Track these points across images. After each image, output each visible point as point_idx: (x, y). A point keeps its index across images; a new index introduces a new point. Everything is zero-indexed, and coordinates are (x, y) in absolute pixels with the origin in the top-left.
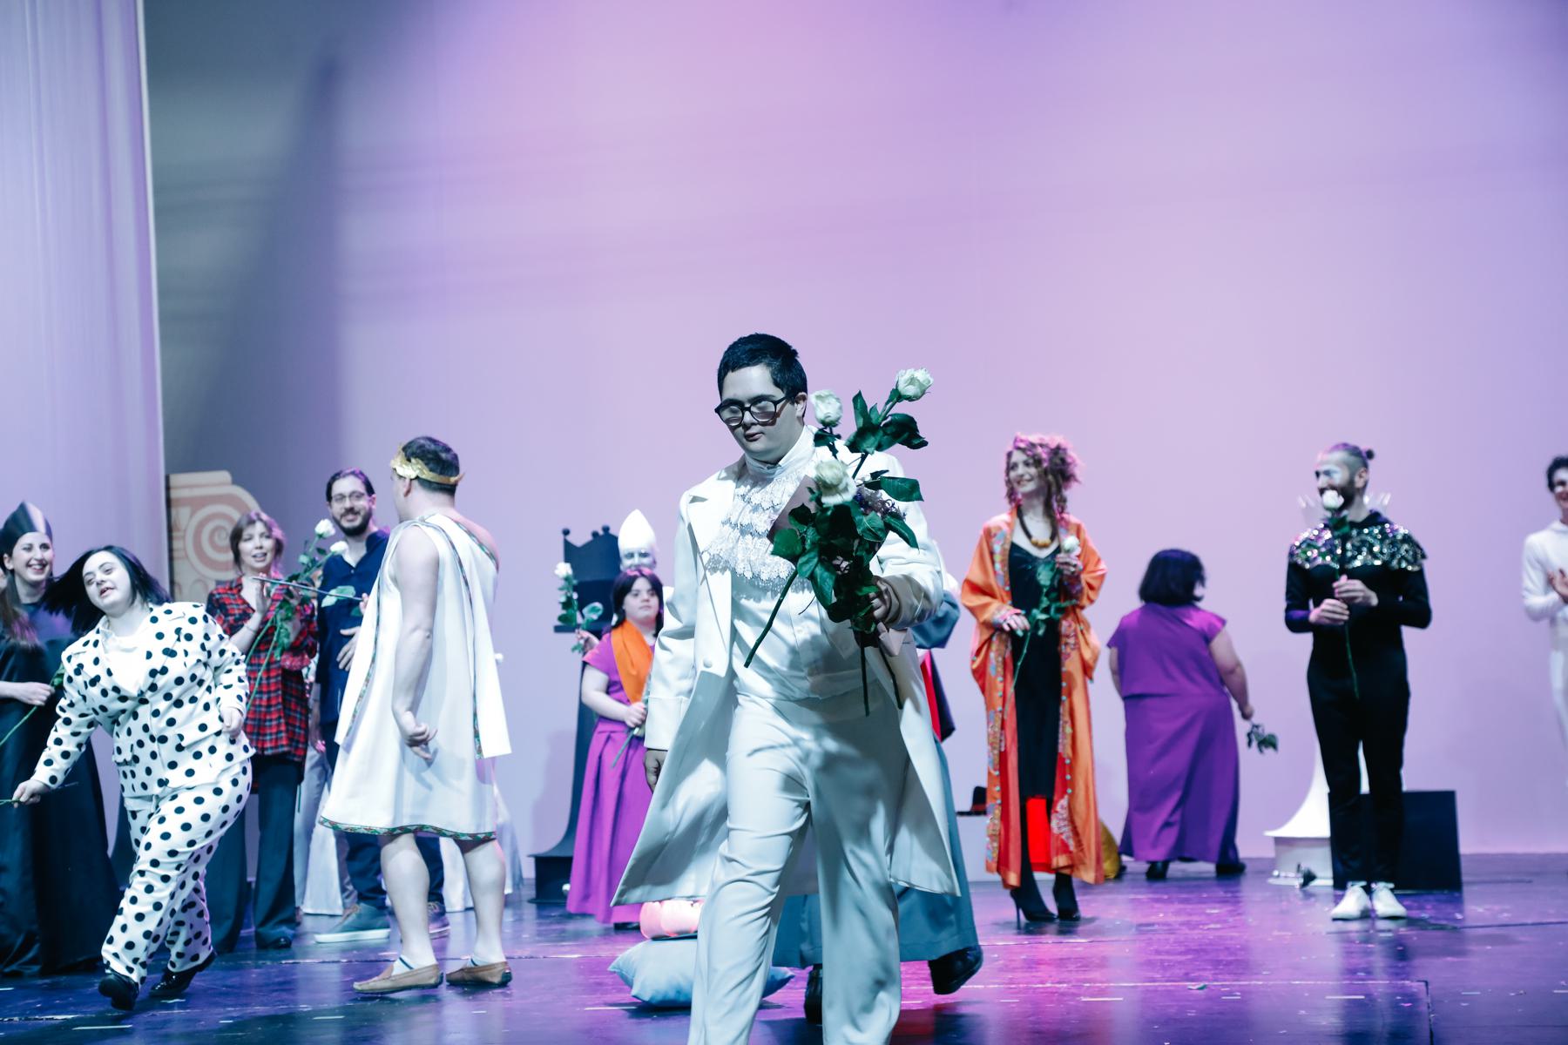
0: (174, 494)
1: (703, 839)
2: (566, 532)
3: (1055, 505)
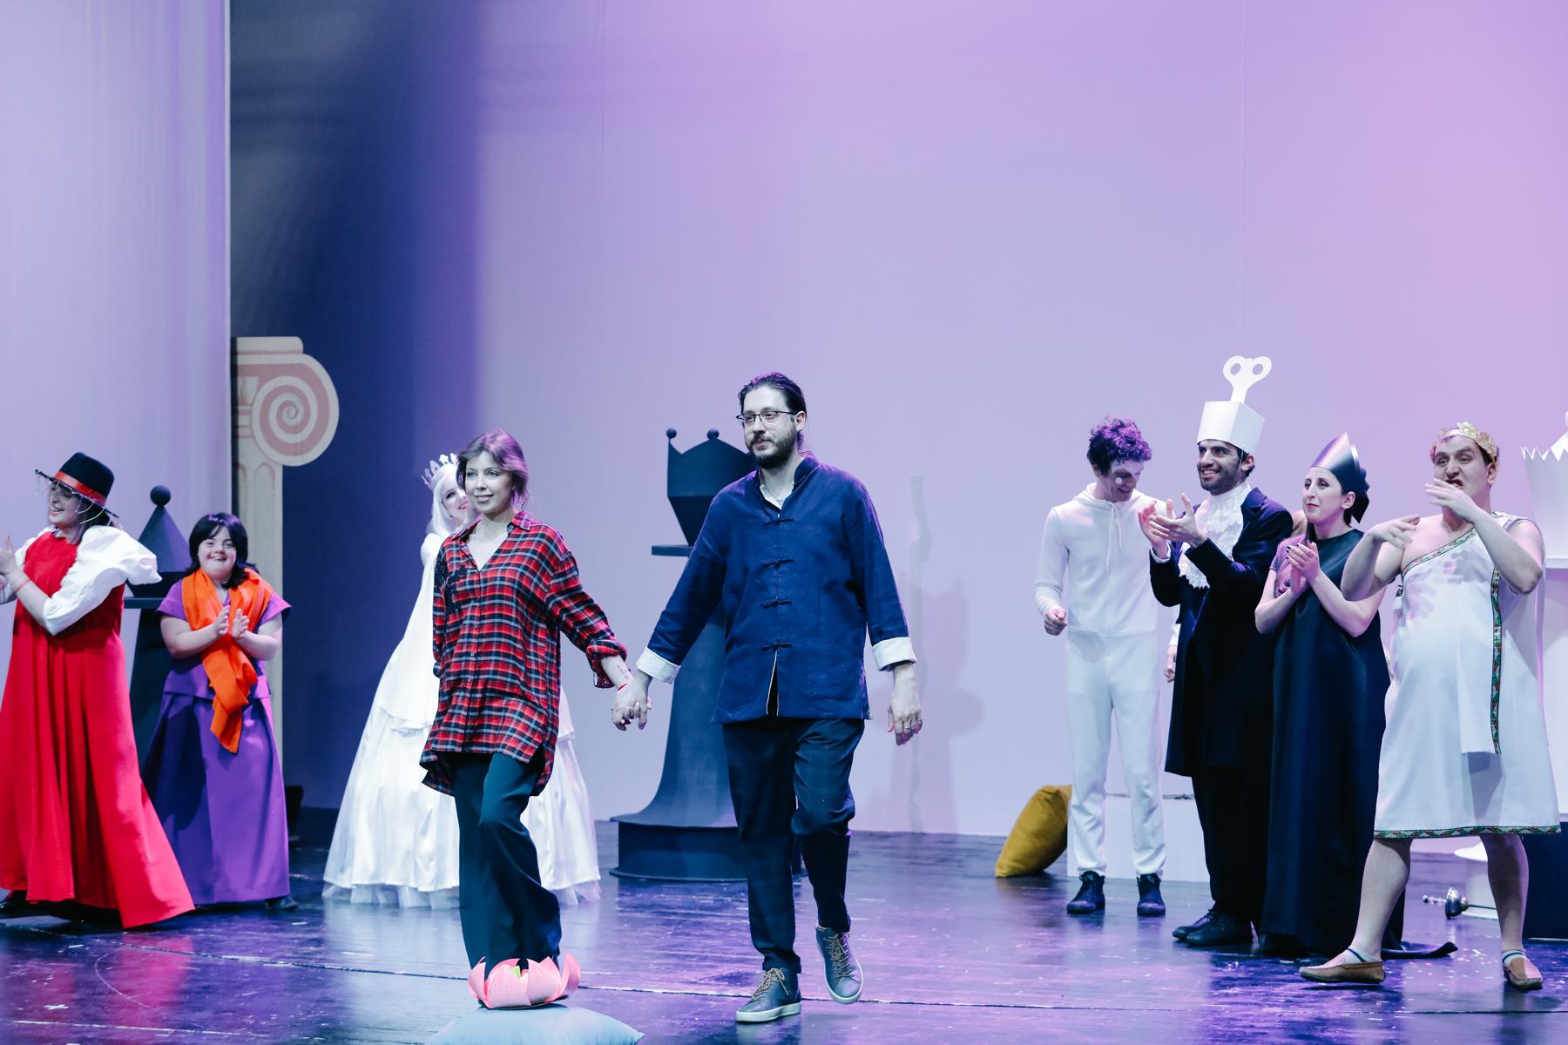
0: (241, 360)
2: (672, 434)
3: (1154, 989)
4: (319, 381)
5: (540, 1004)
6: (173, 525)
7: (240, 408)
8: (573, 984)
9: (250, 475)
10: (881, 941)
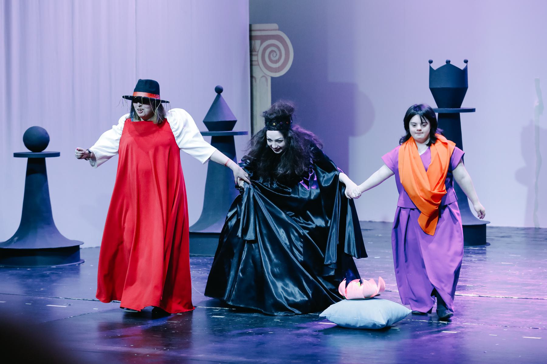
1: (268, 207)
2: (431, 62)
4: (284, 39)
5: (368, 298)
6: (224, 101)
7: (254, 53)
8: (382, 289)
9: (258, 81)
10: (517, 273)
